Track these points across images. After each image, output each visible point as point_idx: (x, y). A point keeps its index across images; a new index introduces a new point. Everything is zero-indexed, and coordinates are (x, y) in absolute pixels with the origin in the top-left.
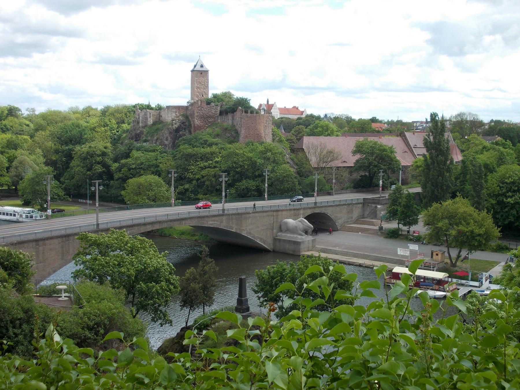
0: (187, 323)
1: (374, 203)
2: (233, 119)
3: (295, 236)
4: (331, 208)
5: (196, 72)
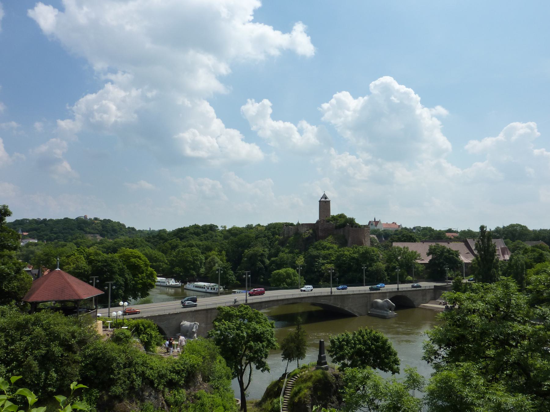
0: (286, 371)
3: (383, 311)
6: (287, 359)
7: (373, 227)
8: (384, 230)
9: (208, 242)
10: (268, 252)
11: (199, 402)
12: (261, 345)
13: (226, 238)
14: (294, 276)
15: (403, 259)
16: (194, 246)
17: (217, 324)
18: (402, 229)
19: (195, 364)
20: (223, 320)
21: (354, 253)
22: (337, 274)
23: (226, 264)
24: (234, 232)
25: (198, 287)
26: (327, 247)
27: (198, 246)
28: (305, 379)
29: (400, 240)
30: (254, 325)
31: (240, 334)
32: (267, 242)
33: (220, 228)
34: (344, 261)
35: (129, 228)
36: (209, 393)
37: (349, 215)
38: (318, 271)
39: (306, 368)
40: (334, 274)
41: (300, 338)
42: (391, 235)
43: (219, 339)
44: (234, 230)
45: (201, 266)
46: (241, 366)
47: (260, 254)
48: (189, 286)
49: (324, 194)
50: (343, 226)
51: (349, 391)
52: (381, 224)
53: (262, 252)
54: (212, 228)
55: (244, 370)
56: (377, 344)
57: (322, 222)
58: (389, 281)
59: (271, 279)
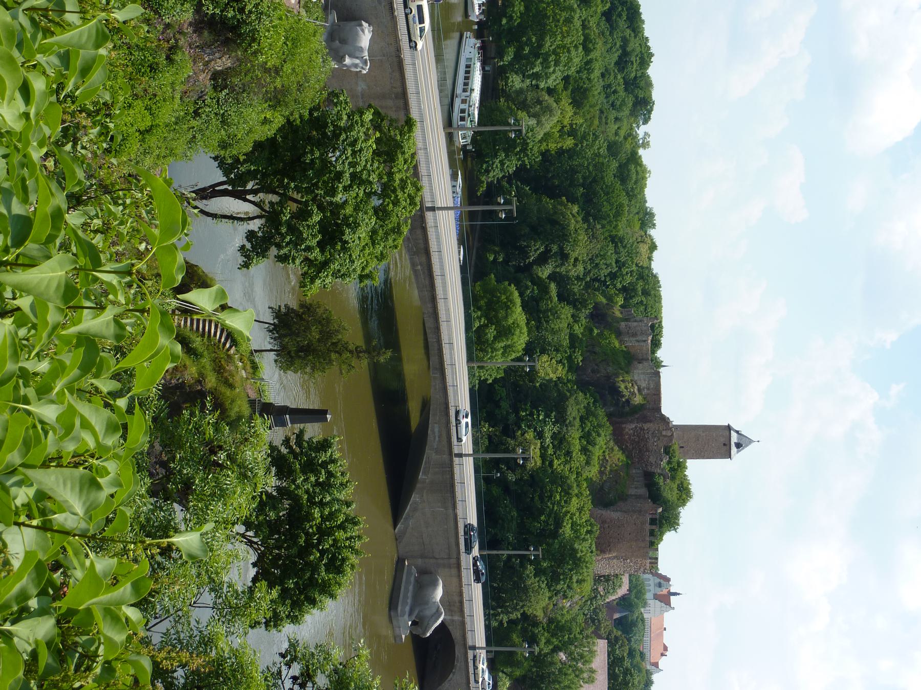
2: (638, 497)
3: (409, 601)
5: (728, 434)
6: (275, 321)
7: (652, 588)
8: (643, 620)
9: (599, 93)
10: (573, 273)
11: (162, 60)
12: (314, 242)
13: (614, 149)
14: (505, 348)
15: (559, 665)
16: (587, 55)
17: (368, 116)
18: (649, 674)
19: (259, 45)
20: (378, 135)
21: (574, 524)
22: (511, 477)
23: (536, 149)
25: (467, 72)
26: (590, 447)
27: (587, 65)
28: (224, 369)
29: (614, 662)
30: (368, 222)
31: (340, 183)
32: (604, 272)
33: (641, 131)
34: (550, 497)
36: (185, 88)
37: (686, 513)
38: (519, 420)
39: (254, 373)
40: (512, 464)
41: (334, 356)
42: (629, 640)
43: (326, 125)
44: (637, 172)
45: (529, 77)
46: (254, 192)
47: (568, 249)
48: (471, 47)
49: (750, 441)
50: (655, 496)
51: (209, 423)
52: (662, 612)
53: (574, 255)
55: (246, 200)
56: (323, 568)
57: (664, 433)
58: (495, 624)
59: (494, 282)
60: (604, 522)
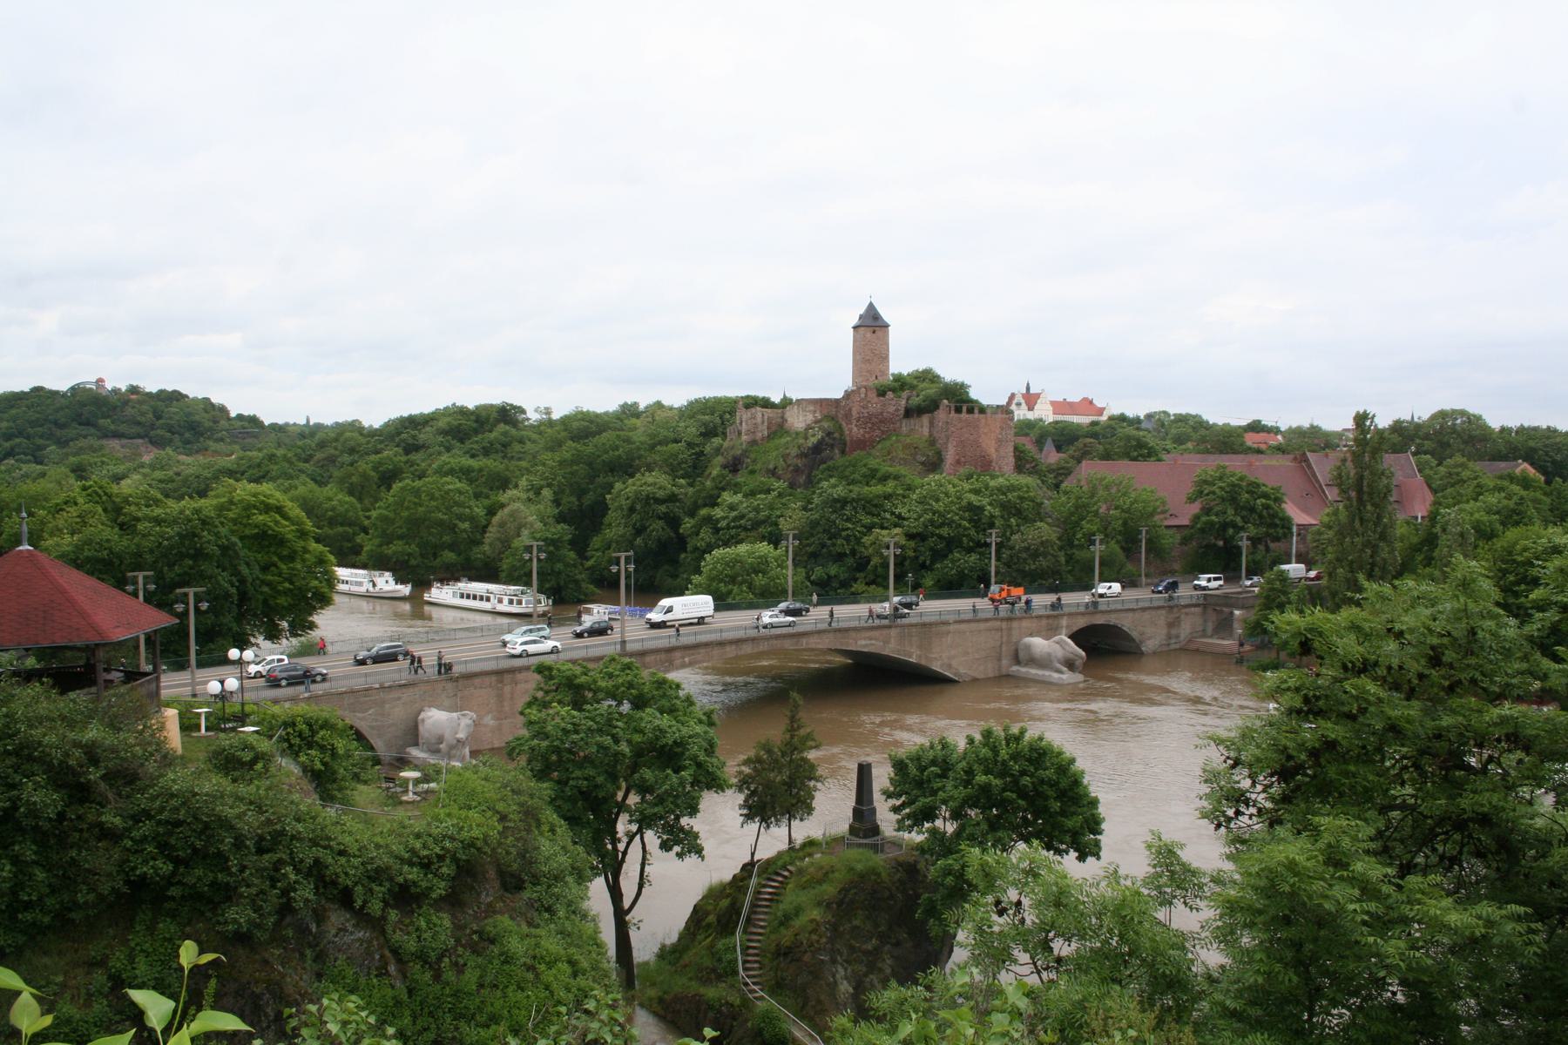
0: (753, 854)
1: (1227, 605)
2: (932, 424)
3: (1047, 673)
4: (1130, 615)
12: (674, 779)
13: (555, 445)
24: (583, 427)
26: (879, 475)
33: (533, 416)
35: (240, 417)
46: (615, 841)
50: (930, 407)
54: (507, 415)
55: (625, 853)
60: (958, 462)
